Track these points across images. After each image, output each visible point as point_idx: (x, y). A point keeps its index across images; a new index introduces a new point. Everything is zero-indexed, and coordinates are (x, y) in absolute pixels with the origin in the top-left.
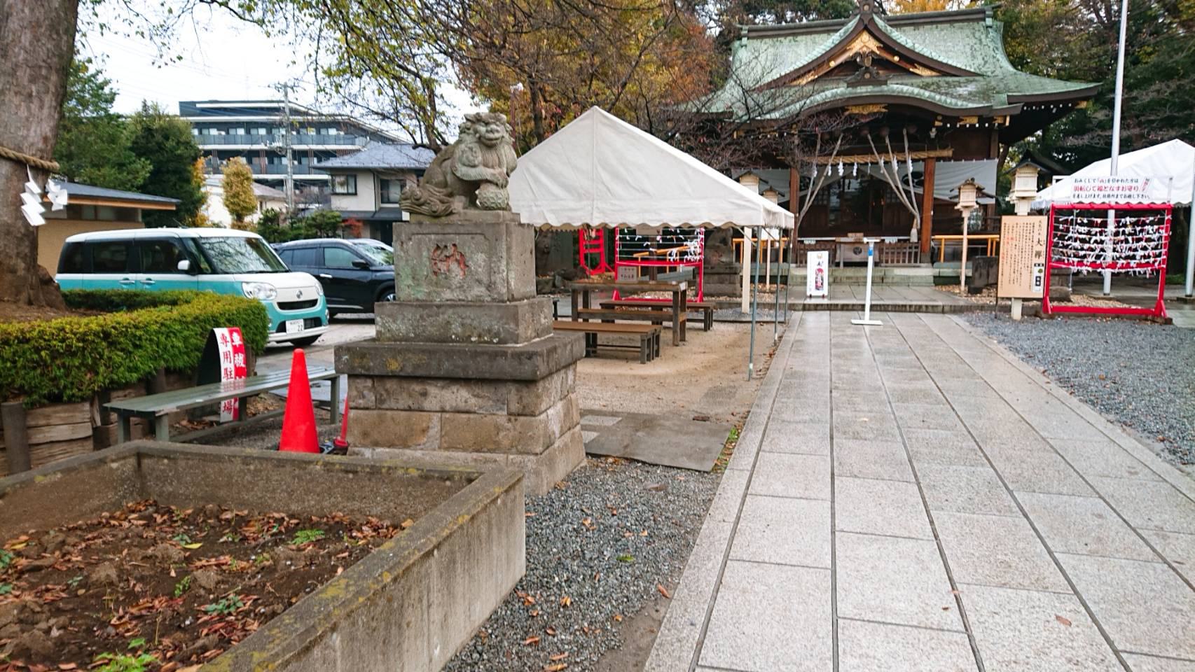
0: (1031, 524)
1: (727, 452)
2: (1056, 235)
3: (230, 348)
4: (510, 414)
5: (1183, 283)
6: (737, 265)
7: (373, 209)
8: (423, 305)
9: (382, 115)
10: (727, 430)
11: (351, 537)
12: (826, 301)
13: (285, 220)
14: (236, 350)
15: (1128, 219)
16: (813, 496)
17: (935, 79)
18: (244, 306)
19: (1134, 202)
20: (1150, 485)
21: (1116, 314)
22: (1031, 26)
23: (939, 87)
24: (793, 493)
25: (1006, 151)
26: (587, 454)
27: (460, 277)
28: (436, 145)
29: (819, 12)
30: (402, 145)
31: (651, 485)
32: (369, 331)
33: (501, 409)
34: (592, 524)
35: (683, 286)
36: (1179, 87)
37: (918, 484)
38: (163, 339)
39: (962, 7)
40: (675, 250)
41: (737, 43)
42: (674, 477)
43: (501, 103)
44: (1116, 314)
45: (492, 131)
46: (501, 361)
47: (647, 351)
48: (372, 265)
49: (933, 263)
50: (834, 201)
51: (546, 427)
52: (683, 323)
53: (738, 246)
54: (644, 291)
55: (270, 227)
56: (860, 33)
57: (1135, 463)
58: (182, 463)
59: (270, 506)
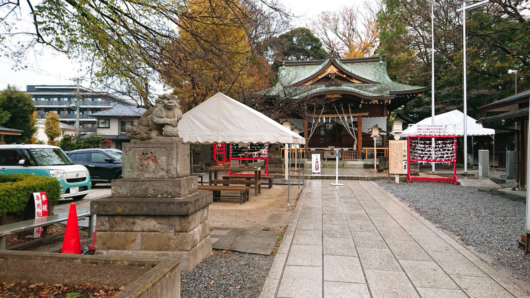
0: (406, 274)
1: (278, 245)
2: (411, 148)
3: (40, 202)
4: (176, 232)
5: (463, 168)
6: (282, 159)
7: (117, 134)
8: (135, 180)
9: (123, 93)
10: (278, 235)
11: (94, 296)
12: (320, 175)
13: (74, 139)
14: (43, 203)
15: (440, 142)
16: (314, 265)
17: (361, 85)
18: (48, 181)
19: (442, 134)
20: (454, 255)
21: (438, 181)
22: (398, 64)
23: (362, 87)
24: (306, 263)
25: (390, 114)
26: (213, 249)
27: (153, 167)
28: (148, 106)
29: (314, 57)
30: (133, 106)
31: (242, 263)
32: (106, 193)
33: (172, 229)
34: (213, 284)
35: (259, 169)
36: (456, 89)
37: (359, 257)
38: (7, 198)
39: (371, 56)
40: (256, 153)
41: (281, 68)
42: (253, 259)
43: (179, 89)
44: (438, 181)
45: (170, 103)
46: (172, 206)
47: (243, 198)
48: (114, 161)
49: (363, 159)
50: (323, 132)
51: (193, 237)
52: (259, 185)
53: (283, 151)
54: (242, 171)
55: (67, 144)
56: (329, 66)
57: (448, 246)
58: (10, 260)
59: (54, 280)
